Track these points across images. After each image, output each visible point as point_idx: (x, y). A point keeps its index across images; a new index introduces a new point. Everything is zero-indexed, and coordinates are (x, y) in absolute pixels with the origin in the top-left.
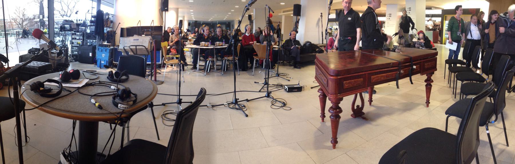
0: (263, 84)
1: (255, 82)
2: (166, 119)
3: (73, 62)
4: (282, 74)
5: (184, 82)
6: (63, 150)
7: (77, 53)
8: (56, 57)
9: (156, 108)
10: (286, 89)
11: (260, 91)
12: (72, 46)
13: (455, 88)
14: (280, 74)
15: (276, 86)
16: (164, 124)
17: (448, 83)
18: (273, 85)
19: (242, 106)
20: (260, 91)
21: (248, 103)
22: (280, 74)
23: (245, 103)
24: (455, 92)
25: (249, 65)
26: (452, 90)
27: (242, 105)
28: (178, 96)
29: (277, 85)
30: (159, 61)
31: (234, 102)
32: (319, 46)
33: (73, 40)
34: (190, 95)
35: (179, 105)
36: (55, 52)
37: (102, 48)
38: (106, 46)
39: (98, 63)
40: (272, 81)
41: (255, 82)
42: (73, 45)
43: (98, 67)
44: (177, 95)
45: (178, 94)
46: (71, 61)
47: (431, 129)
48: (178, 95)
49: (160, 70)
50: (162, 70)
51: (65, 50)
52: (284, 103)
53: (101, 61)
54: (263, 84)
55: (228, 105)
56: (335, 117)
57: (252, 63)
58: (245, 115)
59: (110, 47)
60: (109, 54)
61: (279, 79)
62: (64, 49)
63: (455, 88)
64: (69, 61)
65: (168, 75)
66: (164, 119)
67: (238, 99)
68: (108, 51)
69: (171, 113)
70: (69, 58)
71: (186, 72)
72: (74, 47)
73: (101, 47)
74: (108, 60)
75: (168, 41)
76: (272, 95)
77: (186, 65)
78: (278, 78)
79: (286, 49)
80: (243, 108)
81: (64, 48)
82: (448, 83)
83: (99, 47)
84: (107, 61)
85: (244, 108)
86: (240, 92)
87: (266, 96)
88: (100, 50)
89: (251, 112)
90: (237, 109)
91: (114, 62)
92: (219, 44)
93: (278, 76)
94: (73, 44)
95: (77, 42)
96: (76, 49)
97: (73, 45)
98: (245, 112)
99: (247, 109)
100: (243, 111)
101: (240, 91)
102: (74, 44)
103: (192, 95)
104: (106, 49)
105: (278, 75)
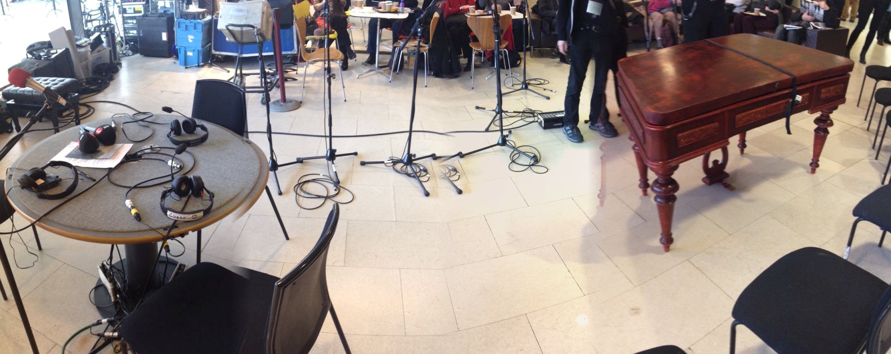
0: (493, 110)
1: (477, 108)
2: (302, 194)
3: (129, 55)
4: (535, 80)
5: (345, 101)
6: (102, 262)
7: (135, 32)
8: (89, 53)
9: (284, 171)
10: (541, 122)
11: (487, 130)
12: (124, 19)
13: (881, 133)
14: (531, 80)
15: (521, 114)
16: (298, 204)
17: (865, 120)
18: (514, 112)
19: (421, 170)
20: (487, 130)
21: (462, 160)
22: (531, 80)
23: (428, 163)
24: (878, 144)
25: (463, 61)
26: (873, 138)
27: (422, 168)
28: (328, 139)
29: (524, 112)
30: (292, 48)
31: (405, 161)
32: (633, 6)
33: (123, 4)
34: (355, 135)
35: (330, 162)
36: (84, 45)
37: (188, 21)
38: (195, 16)
39: (181, 55)
40: (511, 103)
41: (477, 108)
42: (125, 15)
43: (181, 64)
44: (324, 135)
45: (328, 134)
46: (124, 54)
47: (821, 254)
48: (326, 136)
49: (294, 70)
50: (301, 70)
51: (107, 32)
52: (535, 157)
53: (186, 53)
54: (493, 110)
55: (392, 164)
56: (664, 200)
57: (468, 55)
58: (455, 190)
59: (204, 17)
60: (203, 34)
61: (528, 96)
62: (105, 31)
63: (881, 133)
64: (120, 54)
65: (313, 81)
66: (299, 195)
67: (414, 156)
68: (200, 27)
69: (314, 180)
70: (118, 48)
71: (351, 74)
72: (127, 19)
73: (183, 20)
74: (200, 49)
75: (213, 15)
76: (511, 139)
77: (352, 54)
78: (526, 93)
79: (542, 17)
80: (423, 173)
81: (105, 29)
82: (864, 118)
83: (180, 20)
84: (198, 51)
85: (425, 173)
86: (422, 133)
87: (498, 144)
88: (183, 26)
89: (438, 187)
90: (409, 175)
91: (213, 52)
92: (391, 6)
93: (526, 88)
94: (126, 13)
95: (134, 9)
96: (132, 23)
97: (125, 15)
98: (424, 184)
99: (429, 178)
100: (421, 182)
101: (422, 130)
102: (128, 12)
103: (358, 135)
104: (195, 24)
105: (526, 86)
